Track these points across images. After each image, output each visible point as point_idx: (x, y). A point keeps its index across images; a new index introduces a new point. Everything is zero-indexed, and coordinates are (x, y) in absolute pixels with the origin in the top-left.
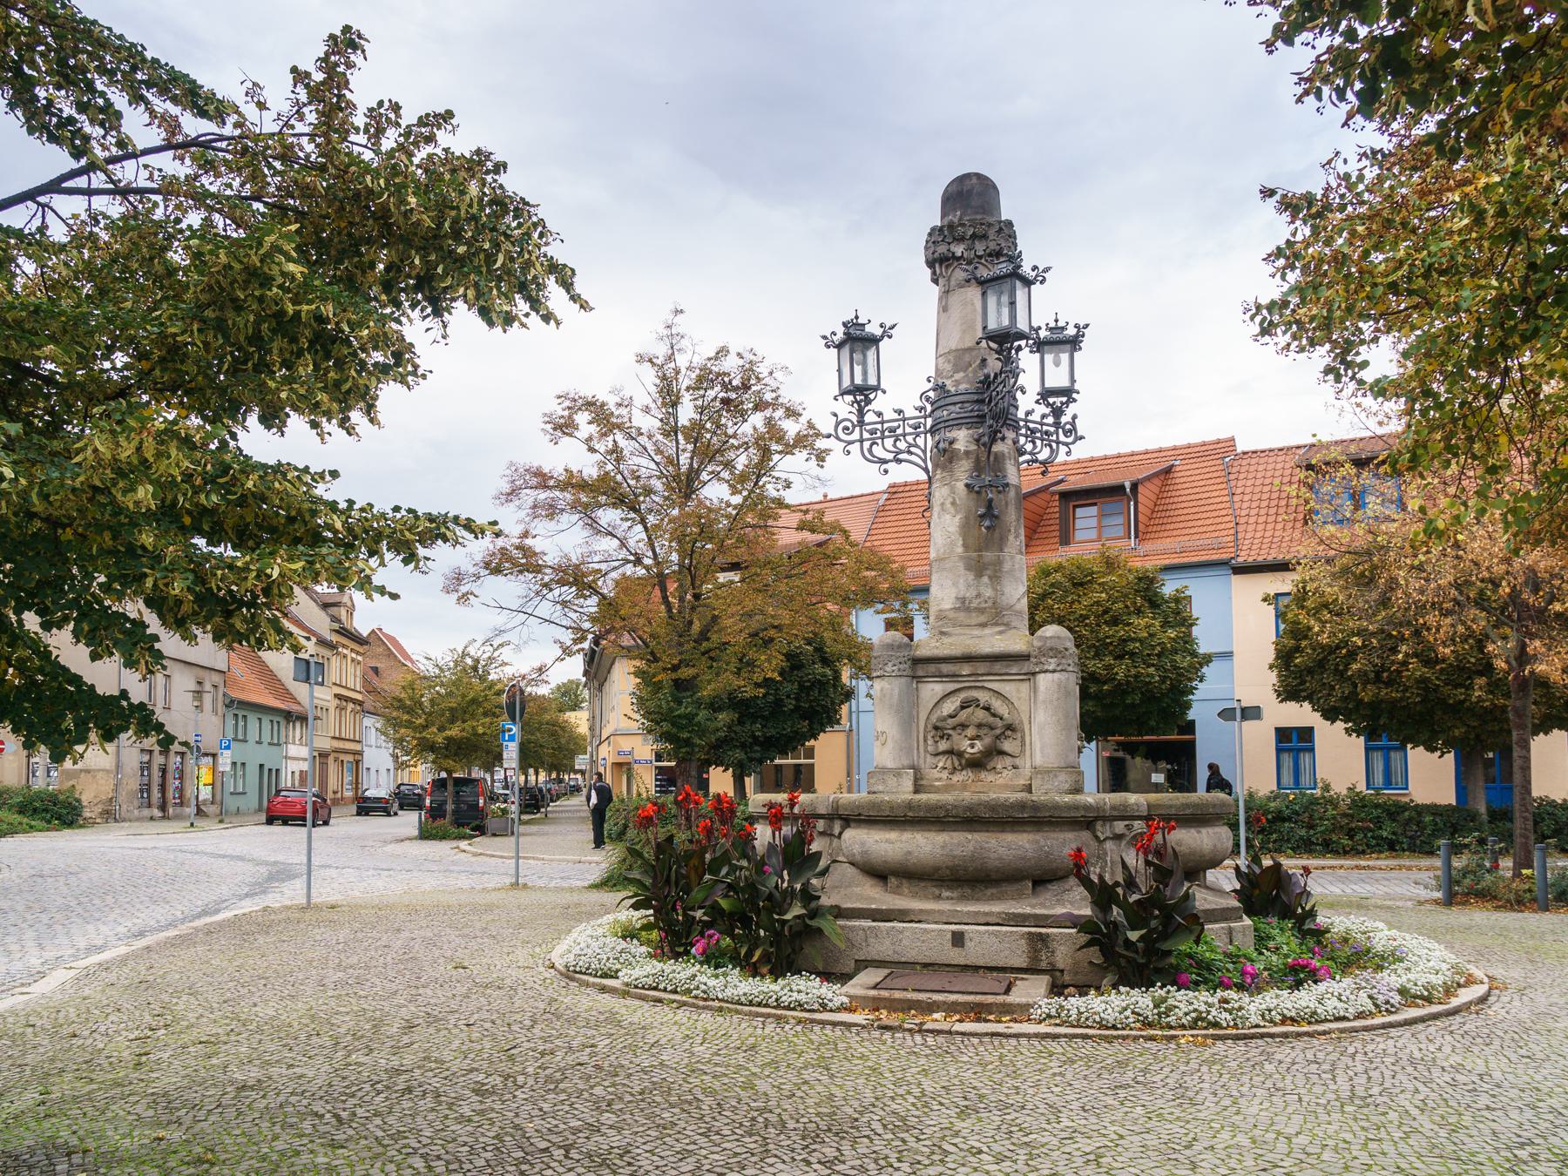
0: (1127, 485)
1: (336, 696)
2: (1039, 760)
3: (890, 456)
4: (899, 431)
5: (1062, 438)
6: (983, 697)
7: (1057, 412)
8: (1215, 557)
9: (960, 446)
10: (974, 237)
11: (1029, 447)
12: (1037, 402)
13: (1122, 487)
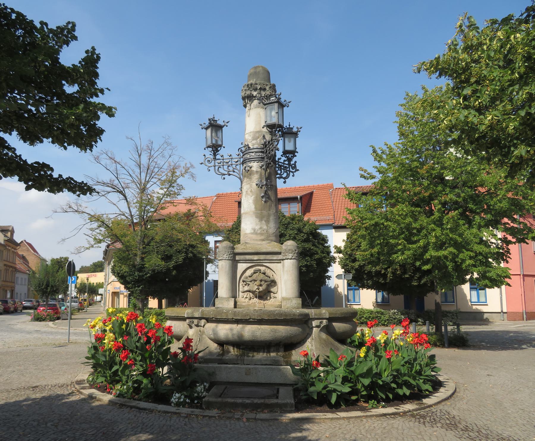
0: (299, 197)
1: (5, 265)
2: (284, 295)
3: (226, 173)
4: (230, 163)
5: (291, 170)
6: (262, 269)
7: (289, 160)
8: (328, 223)
9: (254, 169)
10: (260, 89)
11: (279, 172)
12: (282, 156)
13: (297, 198)
